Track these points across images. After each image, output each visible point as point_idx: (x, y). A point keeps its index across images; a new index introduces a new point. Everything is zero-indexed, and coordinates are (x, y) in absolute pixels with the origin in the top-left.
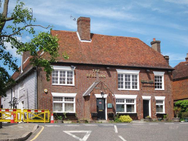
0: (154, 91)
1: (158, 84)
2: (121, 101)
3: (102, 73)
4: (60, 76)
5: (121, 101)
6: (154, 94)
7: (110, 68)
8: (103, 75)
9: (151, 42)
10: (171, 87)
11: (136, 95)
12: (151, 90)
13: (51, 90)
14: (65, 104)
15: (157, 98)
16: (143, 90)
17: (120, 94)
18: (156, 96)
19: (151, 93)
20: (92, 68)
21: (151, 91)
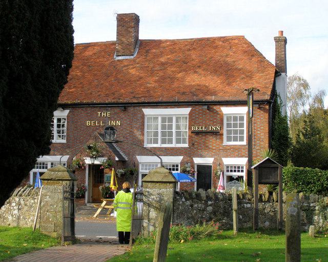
0: (221, 148)
1: (236, 132)
2: (39, 166)
3: (115, 117)
4: (168, 118)
5: (42, 166)
6: (222, 153)
7: (125, 106)
8: (116, 124)
9: (275, 38)
10: (263, 137)
11: (180, 155)
12: (214, 145)
13: (260, 145)
14: (260, 183)
15: (227, 161)
16: (196, 146)
17: (147, 155)
18: (227, 156)
19: (214, 151)
20: (97, 109)
21: (214, 148)
